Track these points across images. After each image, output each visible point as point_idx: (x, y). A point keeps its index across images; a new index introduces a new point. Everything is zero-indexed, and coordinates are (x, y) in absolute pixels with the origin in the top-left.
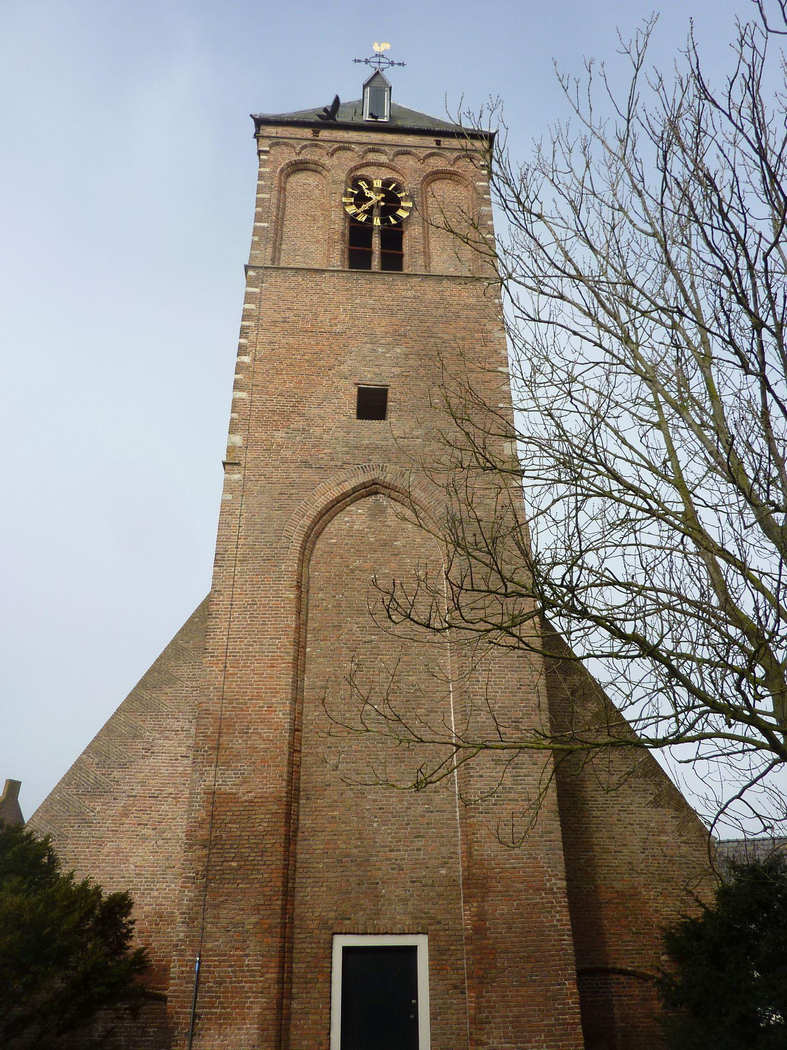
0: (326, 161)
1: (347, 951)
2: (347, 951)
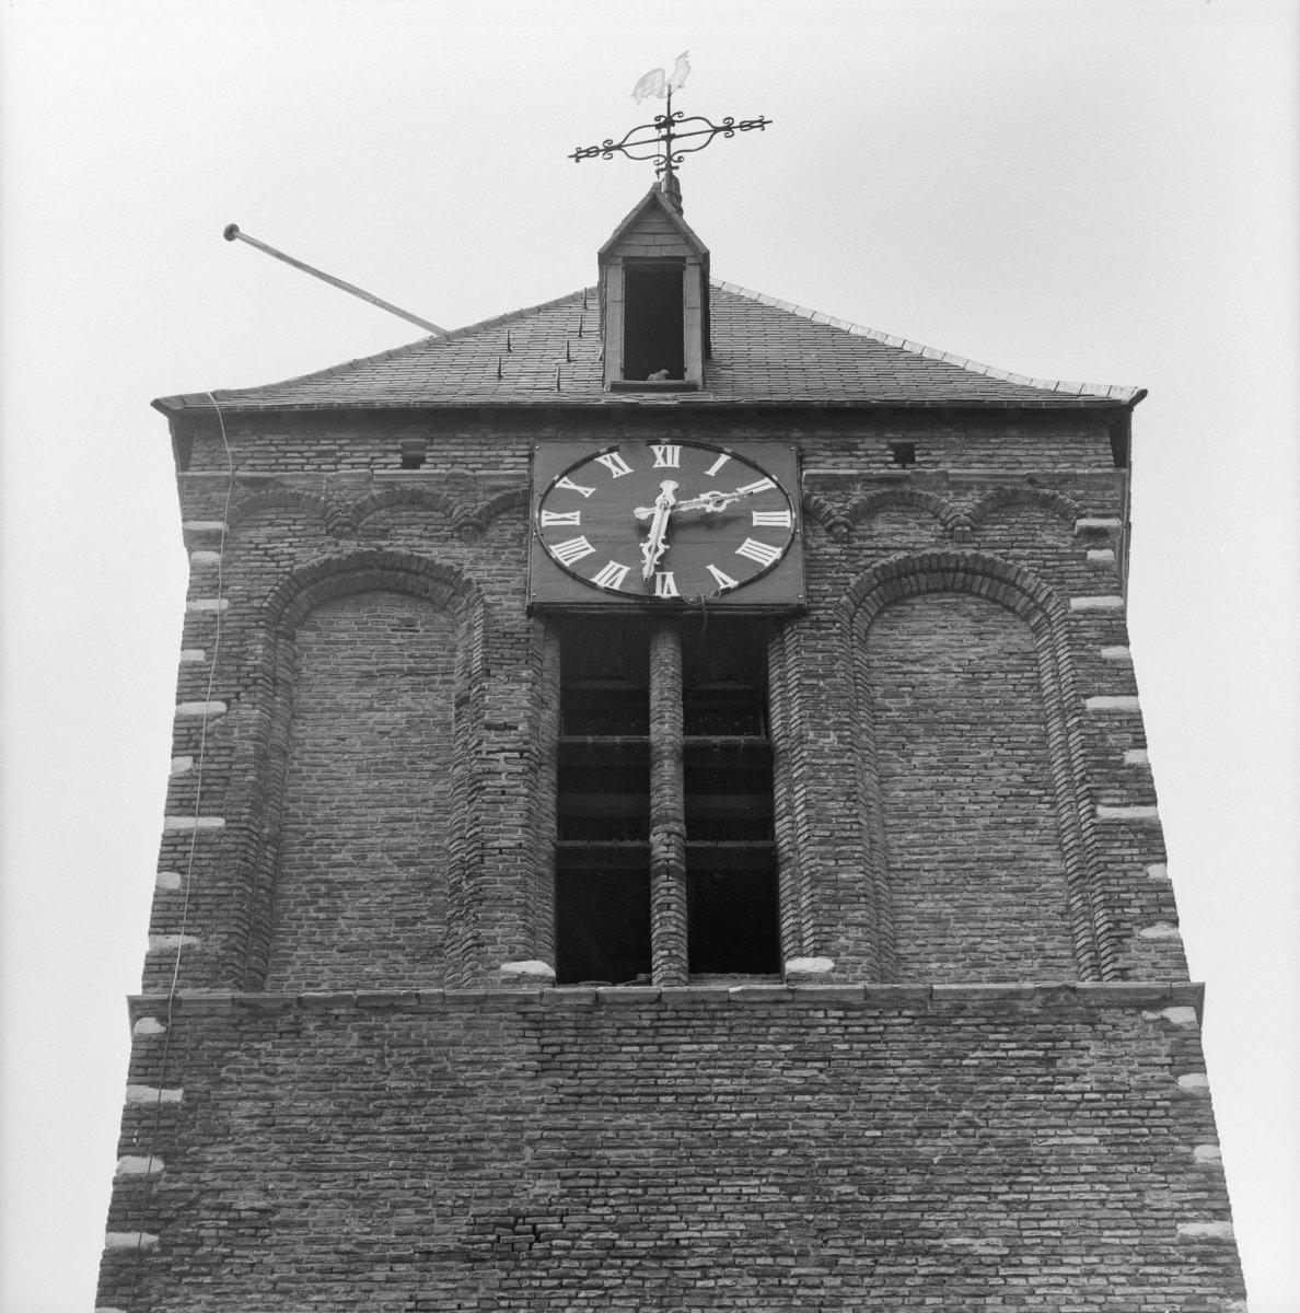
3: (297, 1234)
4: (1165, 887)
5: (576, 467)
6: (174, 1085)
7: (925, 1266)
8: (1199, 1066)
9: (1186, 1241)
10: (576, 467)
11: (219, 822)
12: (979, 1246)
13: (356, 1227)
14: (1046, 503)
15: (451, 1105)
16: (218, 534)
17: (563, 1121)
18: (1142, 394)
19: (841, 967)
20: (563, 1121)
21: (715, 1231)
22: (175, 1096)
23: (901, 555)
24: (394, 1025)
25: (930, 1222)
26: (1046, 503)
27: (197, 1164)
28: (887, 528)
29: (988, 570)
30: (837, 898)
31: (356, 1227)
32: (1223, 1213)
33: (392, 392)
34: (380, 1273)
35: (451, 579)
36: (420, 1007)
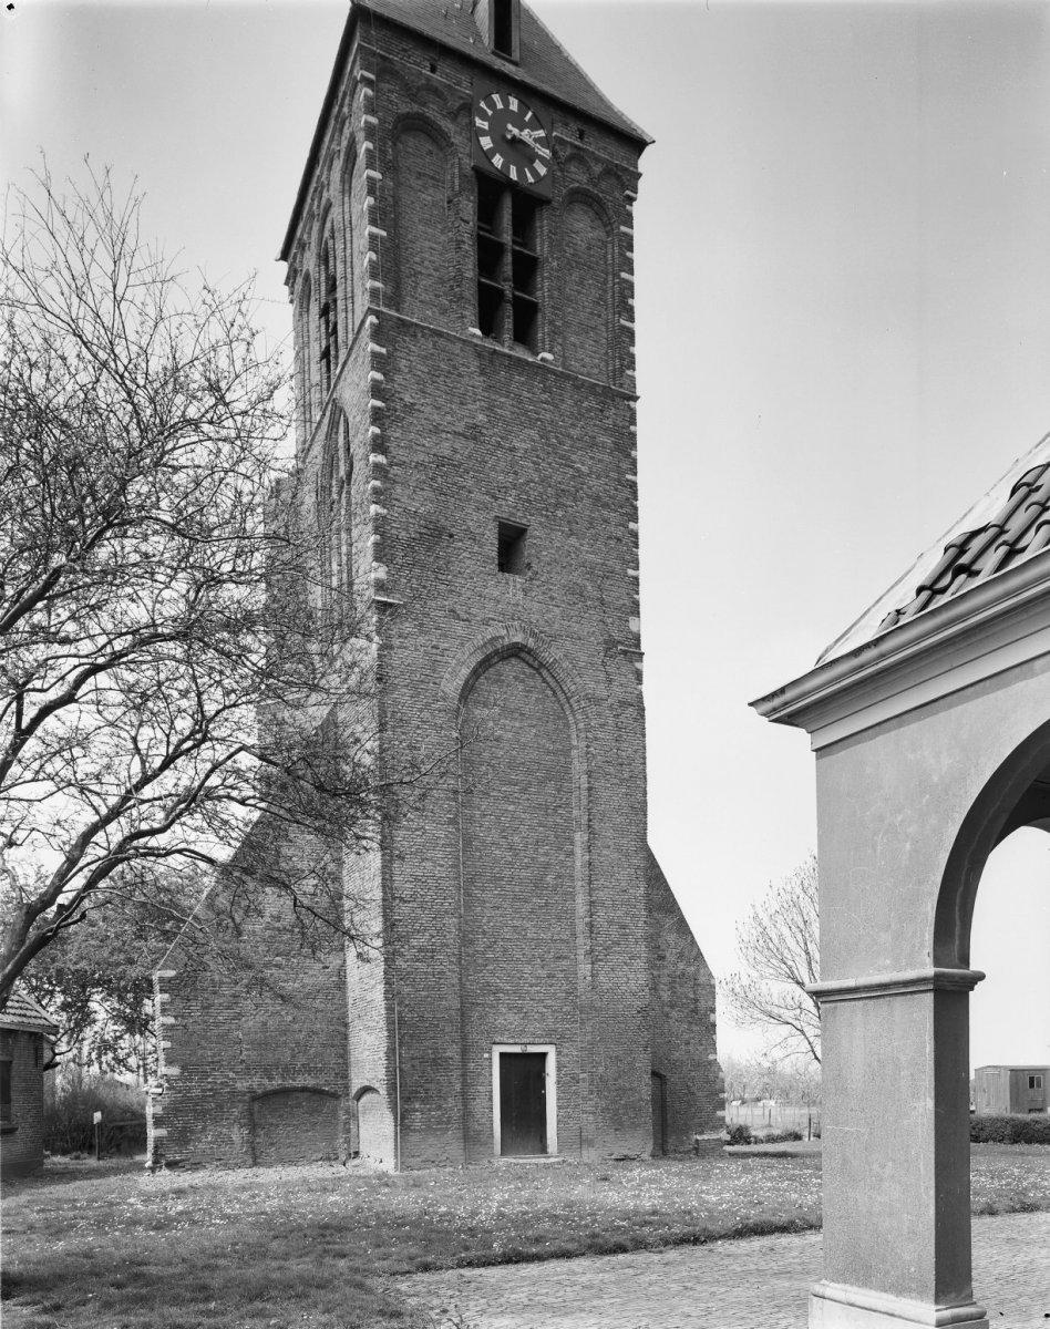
0: (447, 125)
1: (502, 1055)
2: (502, 1055)
3: (421, 415)
4: (633, 356)
5: (537, 118)
6: (383, 346)
7: (571, 471)
8: (635, 424)
9: (628, 480)
10: (537, 118)
11: (384, 234)
12: (583, 468)
13: (436, 417)
14: (618, 178)
15: (458, 379)
16: (372, 81)
17: (486, 394)
18: (654, 142)
19: (555, 359)
20: (486, 394)
21: (524, 446)
22: (384, 351)
23: (577, 185)
24: (442, 342)
25: (573, 457)
26: (618, 178)
27: (393, 380)
28: (573, 169)
29: (599, 201)
30: (555, 332)
31: (436, 417)
32: (635, 474)
33: (1022, 1154)
34: (444, 435)
35: (444, 136)
36: (448, 338)
